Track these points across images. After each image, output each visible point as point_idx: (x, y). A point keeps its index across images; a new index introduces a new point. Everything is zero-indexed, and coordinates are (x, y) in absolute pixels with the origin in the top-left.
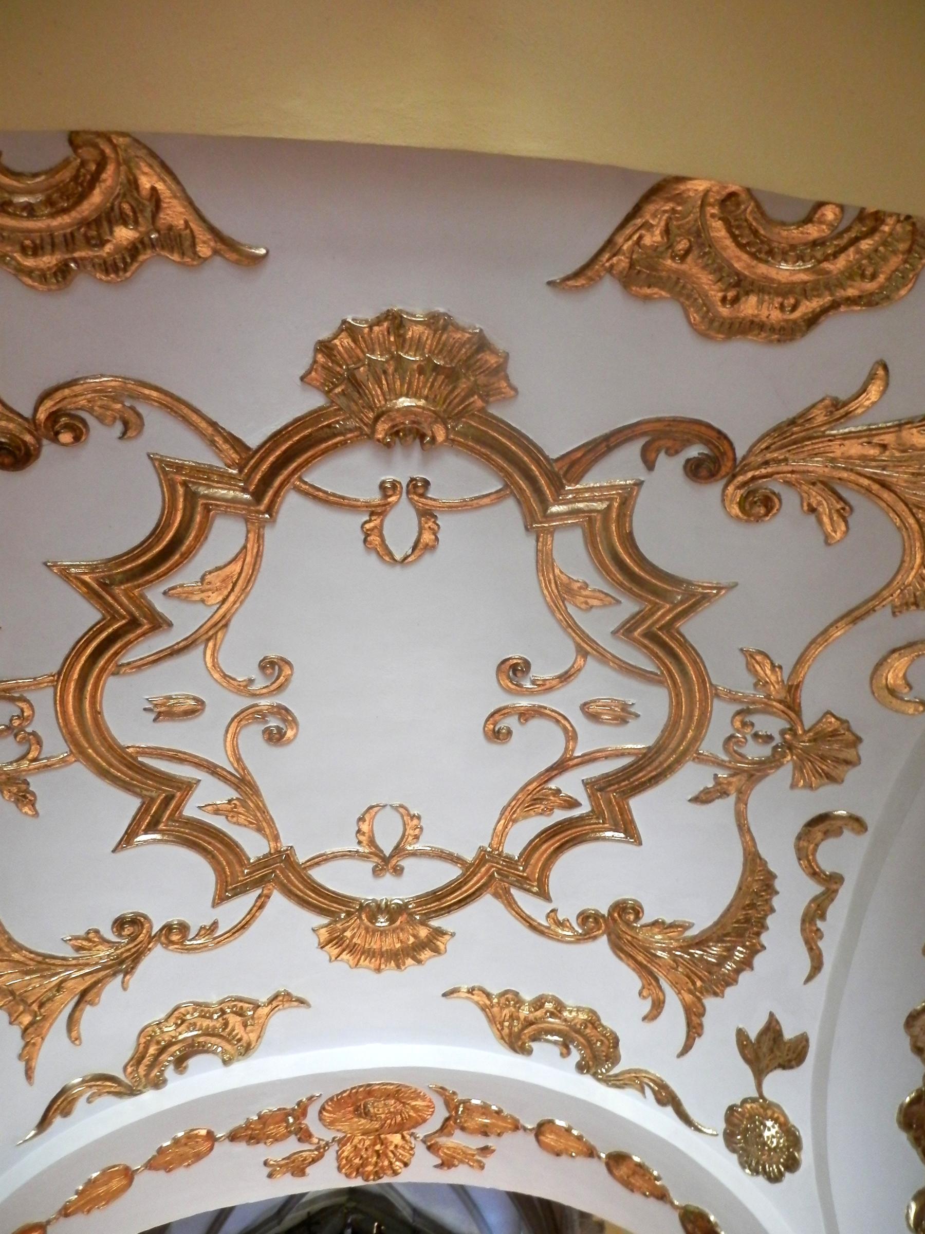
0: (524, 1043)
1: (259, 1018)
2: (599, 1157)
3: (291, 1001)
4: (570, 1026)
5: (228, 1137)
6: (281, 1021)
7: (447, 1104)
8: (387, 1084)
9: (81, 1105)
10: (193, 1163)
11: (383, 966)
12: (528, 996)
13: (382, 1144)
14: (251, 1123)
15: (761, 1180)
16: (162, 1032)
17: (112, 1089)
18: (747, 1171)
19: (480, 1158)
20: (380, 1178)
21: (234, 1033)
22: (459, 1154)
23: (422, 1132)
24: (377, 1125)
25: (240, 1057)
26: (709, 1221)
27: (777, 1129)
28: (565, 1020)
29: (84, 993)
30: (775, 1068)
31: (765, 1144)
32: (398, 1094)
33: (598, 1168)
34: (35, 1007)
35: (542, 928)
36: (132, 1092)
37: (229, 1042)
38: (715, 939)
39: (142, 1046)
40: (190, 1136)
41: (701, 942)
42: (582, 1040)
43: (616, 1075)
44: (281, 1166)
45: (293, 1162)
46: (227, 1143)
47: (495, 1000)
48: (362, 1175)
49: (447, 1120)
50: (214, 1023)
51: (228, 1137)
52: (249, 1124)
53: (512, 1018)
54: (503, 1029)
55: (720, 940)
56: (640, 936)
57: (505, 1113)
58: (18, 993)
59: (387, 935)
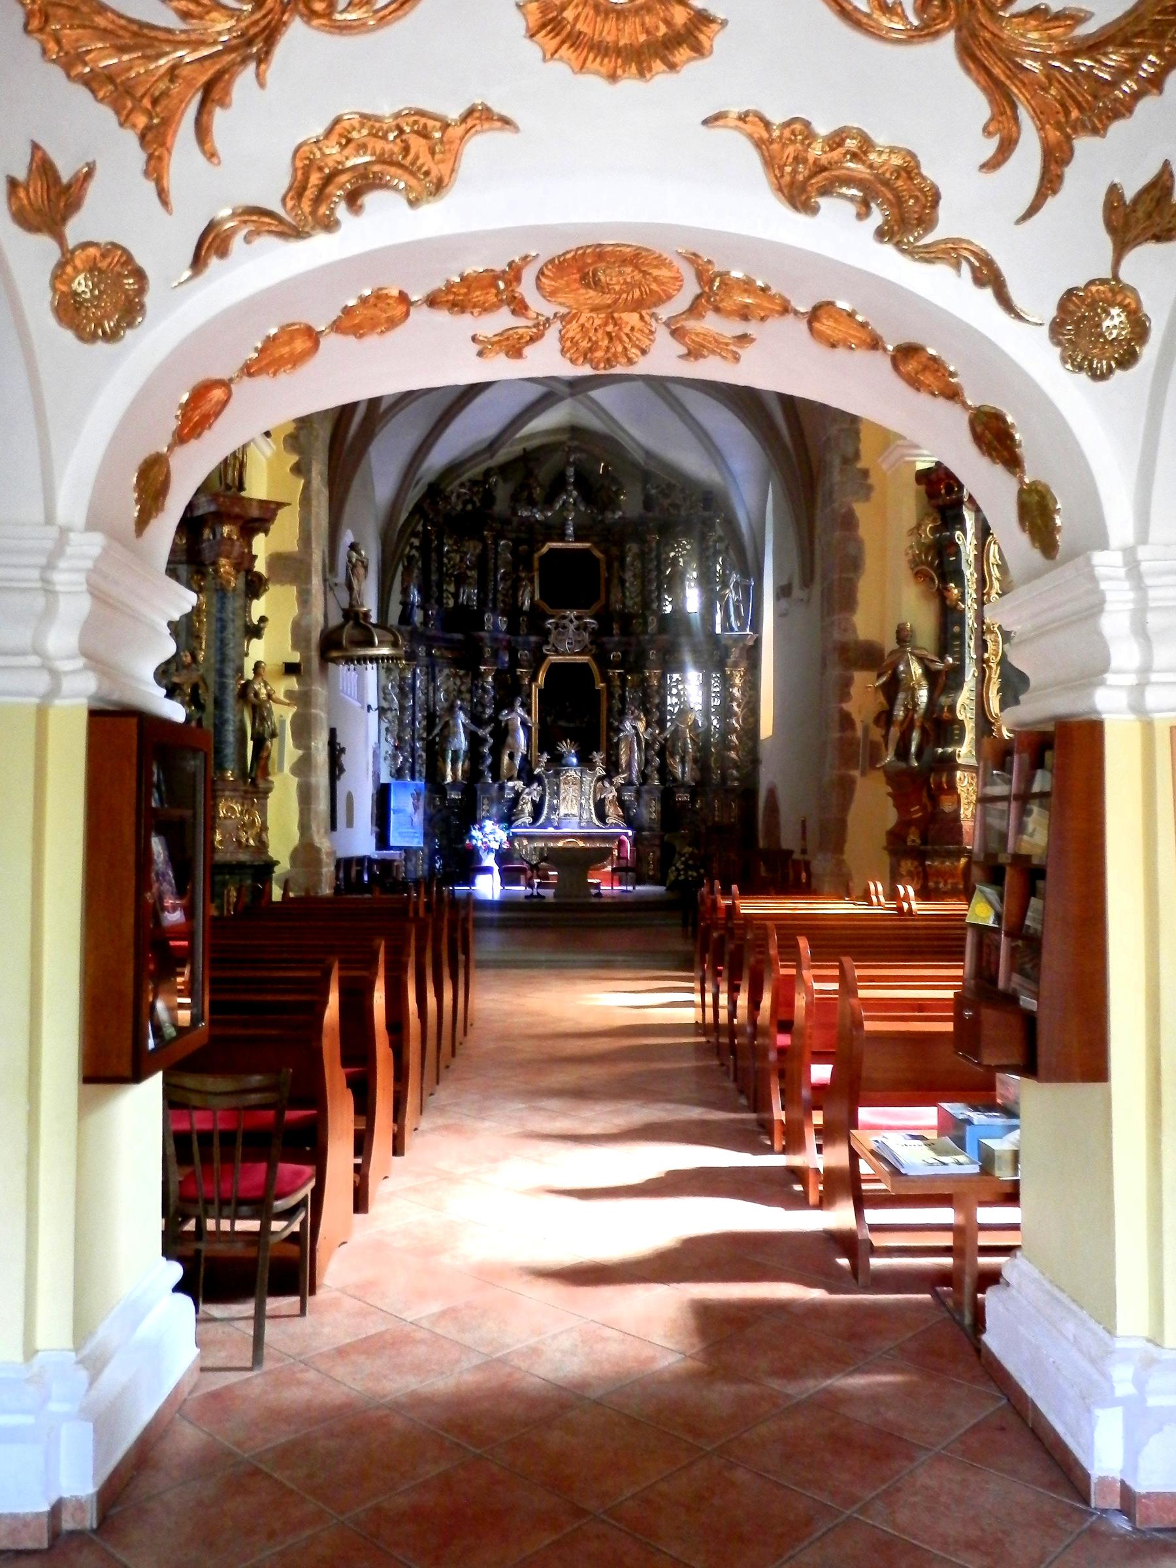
0: (809, 198)
1: (451, 142)
2: (885, 350)
3: (492, 119)
4: (877, 176)
5: (426, 302)
6: (479, 149)
7: (700, 275)
8: (624, 245)
9: (237, 243)
10: (388, 329)
11: (619, 72)
12: (822, 129)
13: (615, 324)
14: (453, 286)
15: (1083, 377)
16: (323, 154)
17: (273, 228)
18: (1069, 366)
19: (735, 349)
20: (612, 367)
21: (419, 163)
22: (710, 342)
23: (665, 312)
24: (608, 299)
25: (431, 198)
26: (1005, 421)
27: (1123, 318)
28: (871, 166)
29: (208, 88)
30: (1146, 240)
31: (1102, 335)
32: (635, 257)
33: (881, 363)
34: (146, 103)
35: (860, 17)
36: (295, 232)
37: (413, 174)
38: (1118, 41)
39: (300, 173)
40: (379, 297)
41: (1095, 46)
42: (890, 196)
43: (926, 246)
44: (492, 344)
45: (508, 339)
46: (425, 308)
47: (776, 133)
48: (591, 361)
49: (698, 297)
50: (391, 146)
51: (426, 302)
52: (450, 286)
53: (797, 160)
54: (782, 176)
55: (1126, 43)
56: (1006, 34)
57: (773, 291)
58: (118, 81)
59: (626, 18)
